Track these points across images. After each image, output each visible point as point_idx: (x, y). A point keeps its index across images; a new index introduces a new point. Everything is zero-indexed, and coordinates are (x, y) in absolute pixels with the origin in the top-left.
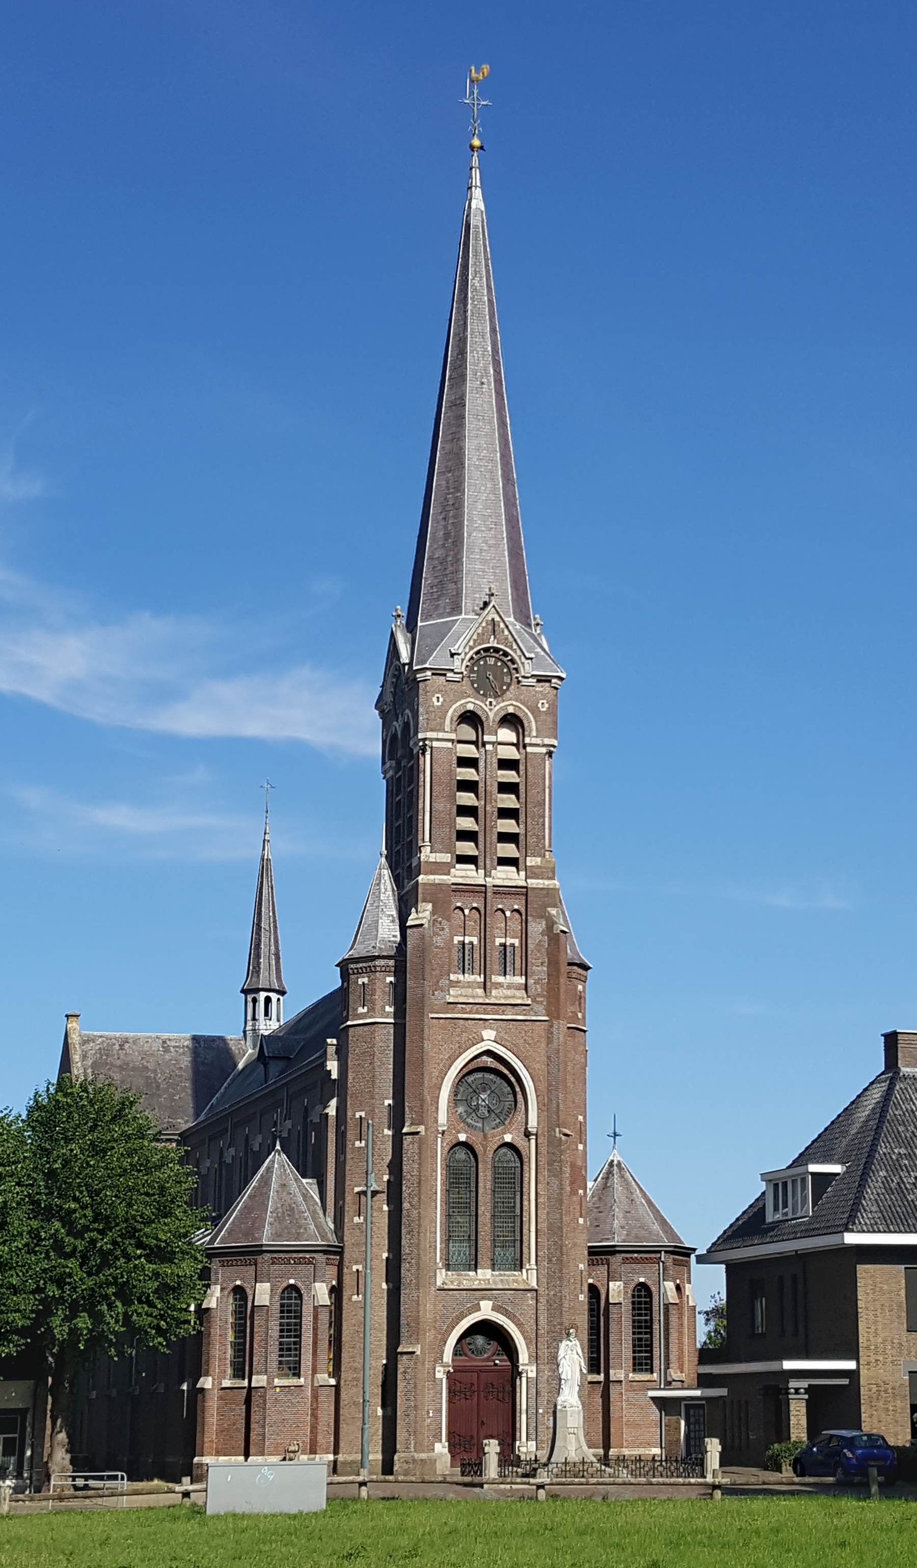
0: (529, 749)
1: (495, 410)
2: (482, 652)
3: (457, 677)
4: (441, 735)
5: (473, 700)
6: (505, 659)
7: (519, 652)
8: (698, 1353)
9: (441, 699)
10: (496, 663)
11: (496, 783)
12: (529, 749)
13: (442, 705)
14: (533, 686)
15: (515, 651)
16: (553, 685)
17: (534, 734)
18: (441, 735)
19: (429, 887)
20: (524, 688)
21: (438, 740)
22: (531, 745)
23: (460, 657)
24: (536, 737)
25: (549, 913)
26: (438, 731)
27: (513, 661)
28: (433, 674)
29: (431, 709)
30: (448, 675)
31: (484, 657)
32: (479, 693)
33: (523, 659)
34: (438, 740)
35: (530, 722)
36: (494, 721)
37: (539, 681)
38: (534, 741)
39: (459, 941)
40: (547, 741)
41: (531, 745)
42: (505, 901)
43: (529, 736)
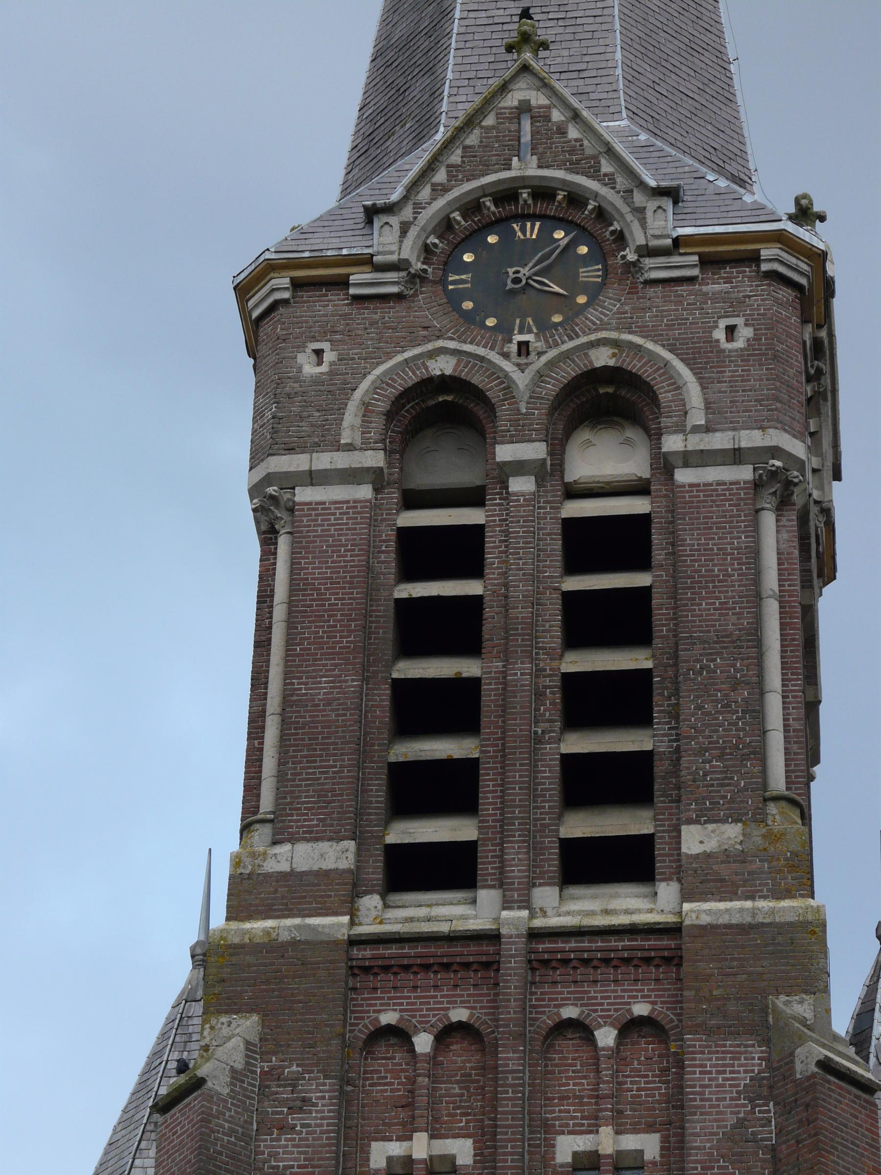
0: (683, 476)
1: (835, 1080)
2: (488, 202)
3: (391, 285)
4: (324, 461)
5: (452, 345)
6: (578, 217)
7: (621, 181)
8: (594, 1149)
9: (329, 356)
10: (546, 236)
11: (557, 596)
12: (683, 476)
13: (331, 373)
14: (691, 280)
15: (609, 181)
16: (764, 267)
17: (698, 418)
18: (324, 461)
19: (249, 959)
20: (651, 291)
21: (313, 478)
22: (689, 459)
23: (394, 221)
24: (708, 429)
25: (775, 1010)
26: (316, 447)
27: (602, 215)
28: (297, 285)
29: (291, 387)
30: (353, 279)
31: (500, 221)
32: (483, 325)
33: (639, 198)
34: (313, 478)
35: (678, 387)
36: (534, 397)
37: (707, 262)
38: (696, 442)
39: (390, 1159)
40: (751, 439)
41: (689, 459)
42: (593, 991)
43: (680, 429)
